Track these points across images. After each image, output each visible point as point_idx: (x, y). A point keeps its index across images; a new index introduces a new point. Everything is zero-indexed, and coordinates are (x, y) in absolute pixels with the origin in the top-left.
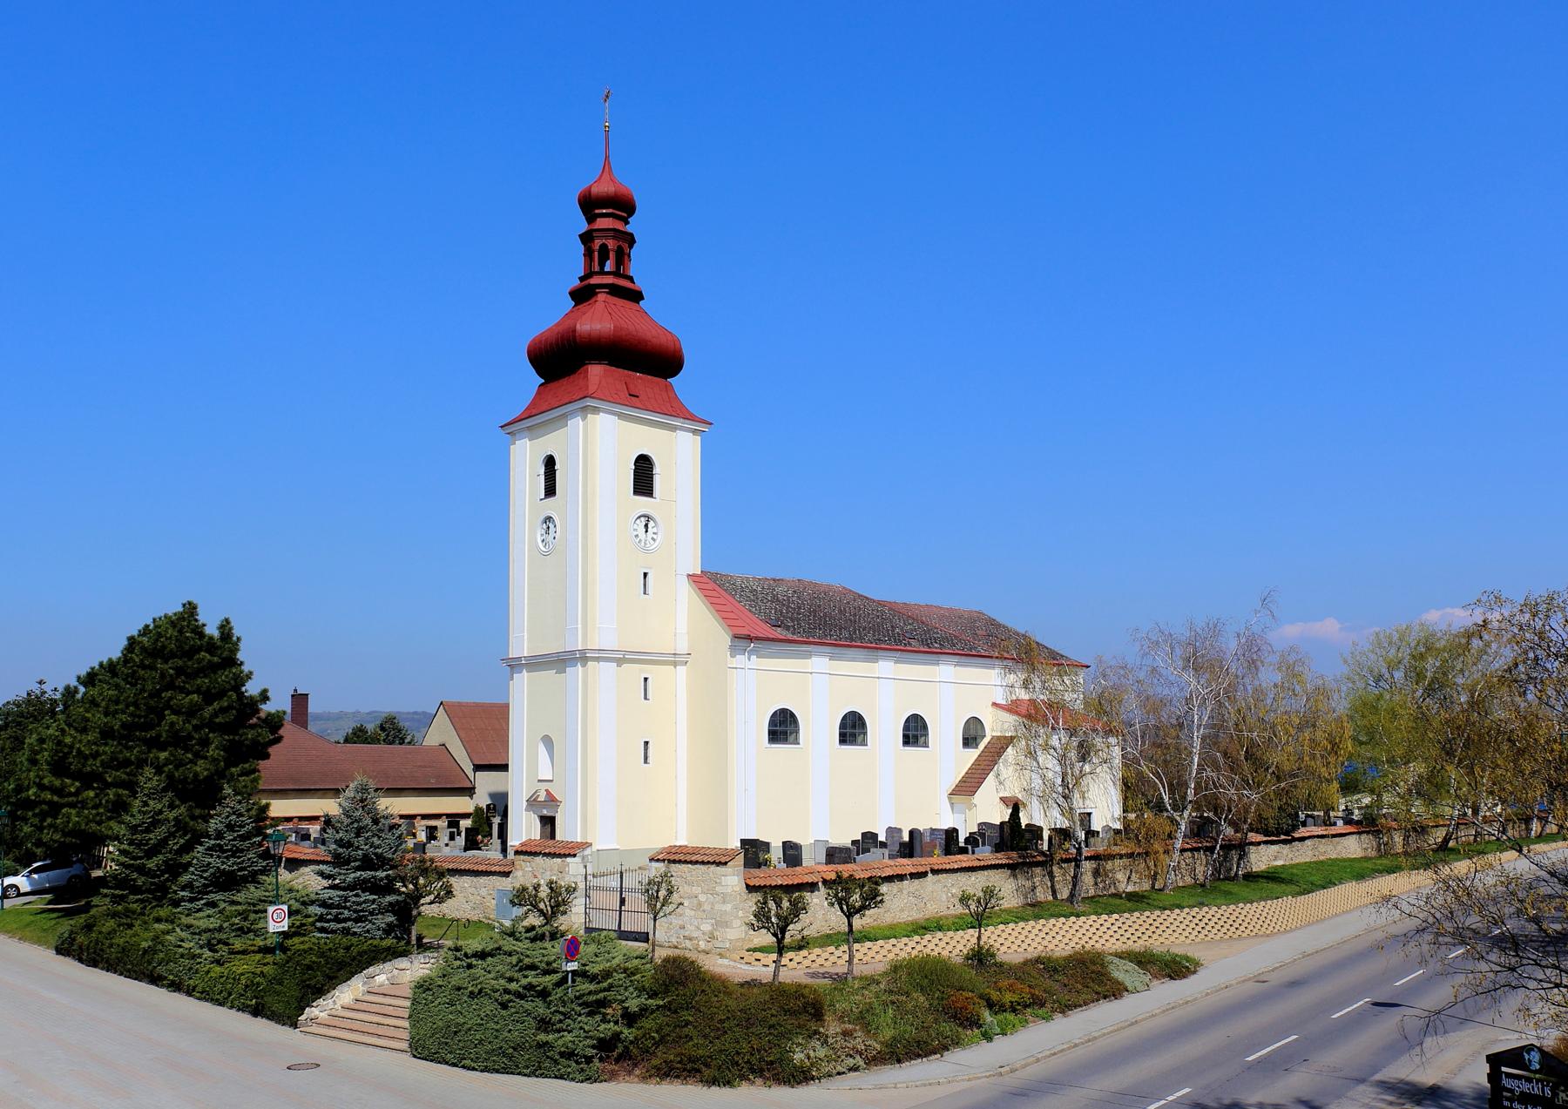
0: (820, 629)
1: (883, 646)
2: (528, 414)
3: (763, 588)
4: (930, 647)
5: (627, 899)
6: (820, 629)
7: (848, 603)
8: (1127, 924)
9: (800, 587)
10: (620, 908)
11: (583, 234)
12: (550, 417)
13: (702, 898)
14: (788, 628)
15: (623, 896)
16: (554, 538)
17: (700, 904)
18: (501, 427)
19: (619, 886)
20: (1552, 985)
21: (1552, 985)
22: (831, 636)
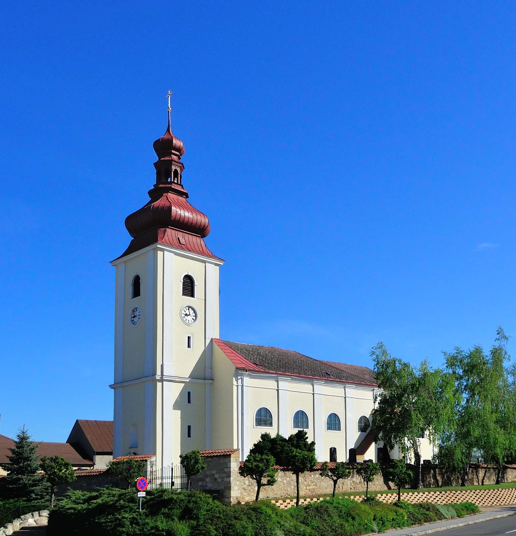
0: (283, 368)
1: (316, 377)
2: (128, 252)
3: (253, 350)
4: (341, 380)
5: (175, 483)
6: (283, 368)
7: (298, 358)
8: (442, 500)
9: (272, 351)
10: (172, 487)
11: (138, 296)
12: (142, 252)
13: (217, 476)
14: (266, 367)
15: (173, 481)
16: (139, 318)
17: (215, 479)
18: (110, 262)
19: (171, 475)
20: (412, 443)
21: (412, 443)
22: (289, 371)
